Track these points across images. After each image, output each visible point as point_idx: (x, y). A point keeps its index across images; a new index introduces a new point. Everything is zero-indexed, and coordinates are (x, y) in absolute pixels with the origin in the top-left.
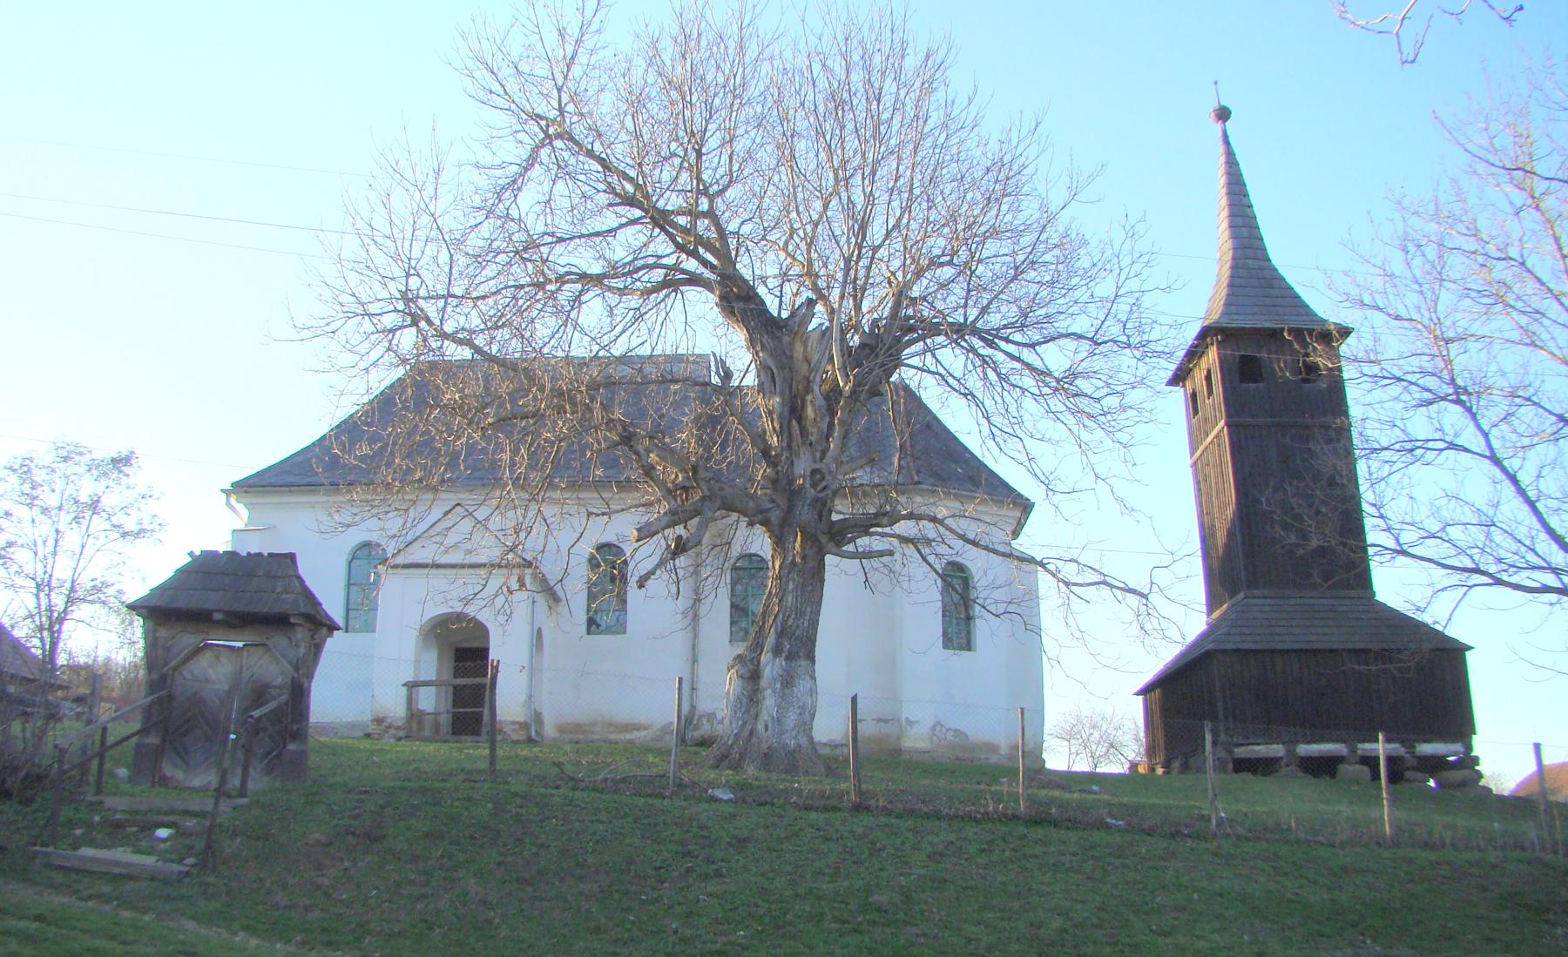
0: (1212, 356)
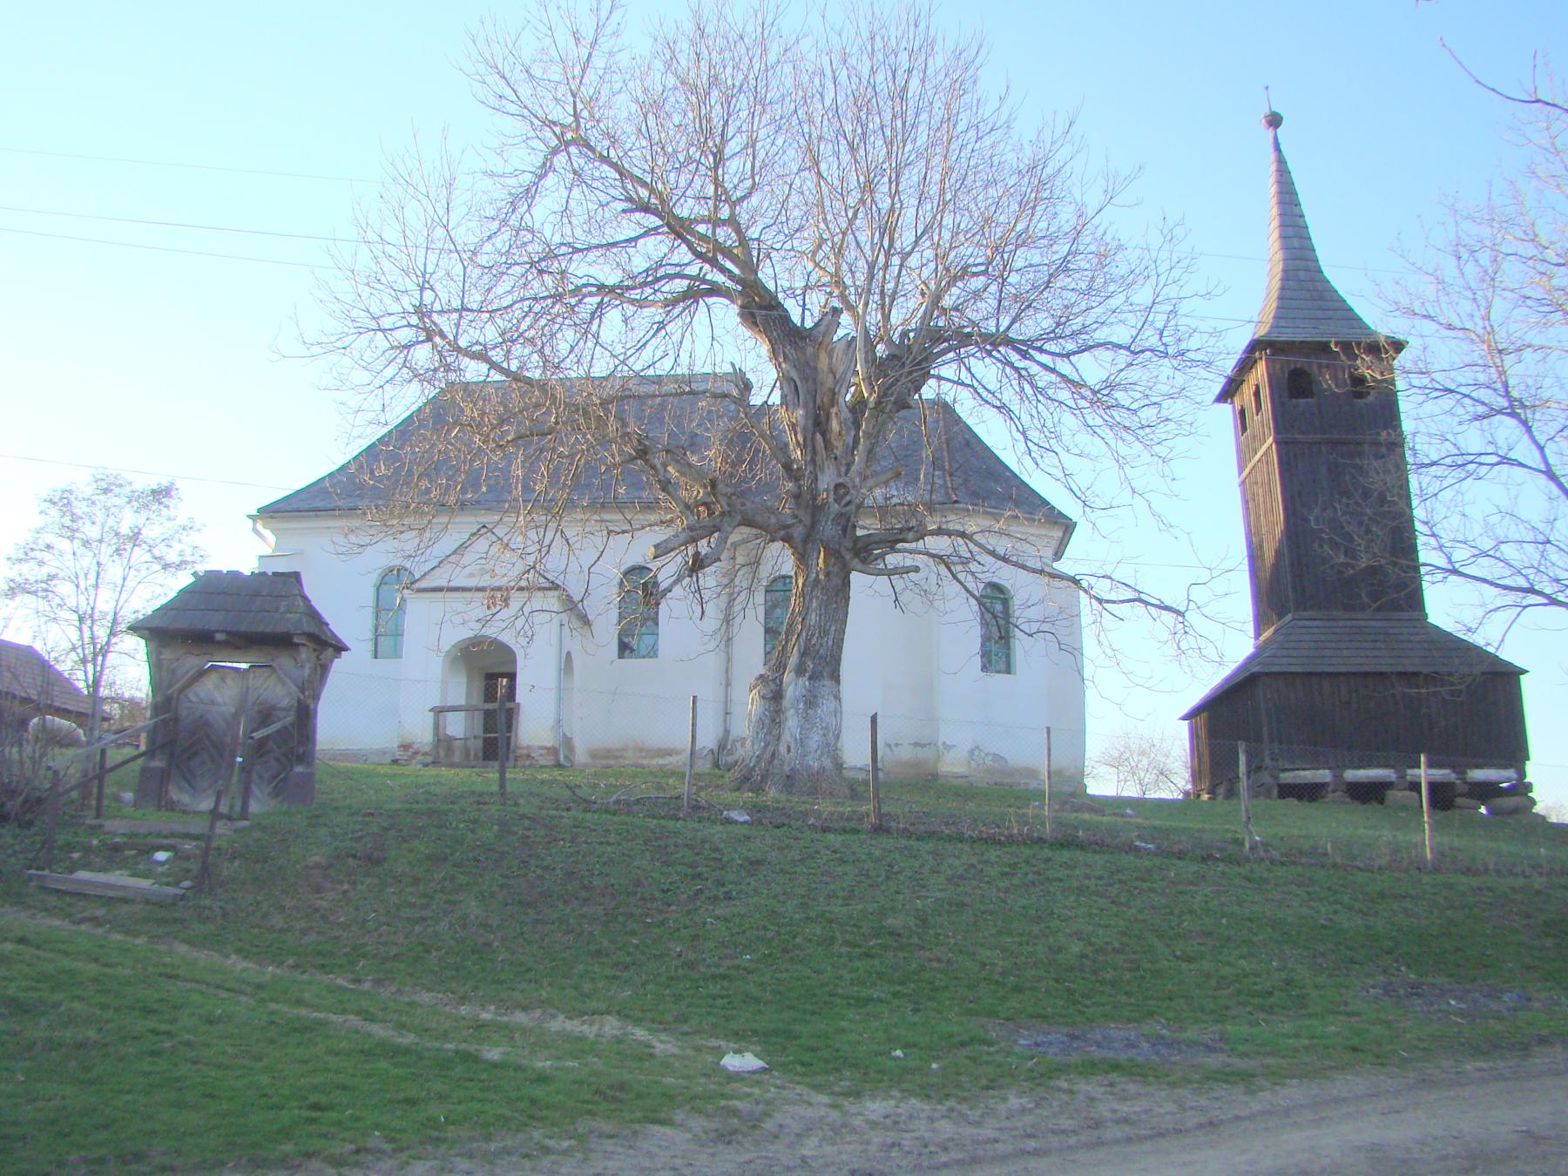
0: (1260, 373)
